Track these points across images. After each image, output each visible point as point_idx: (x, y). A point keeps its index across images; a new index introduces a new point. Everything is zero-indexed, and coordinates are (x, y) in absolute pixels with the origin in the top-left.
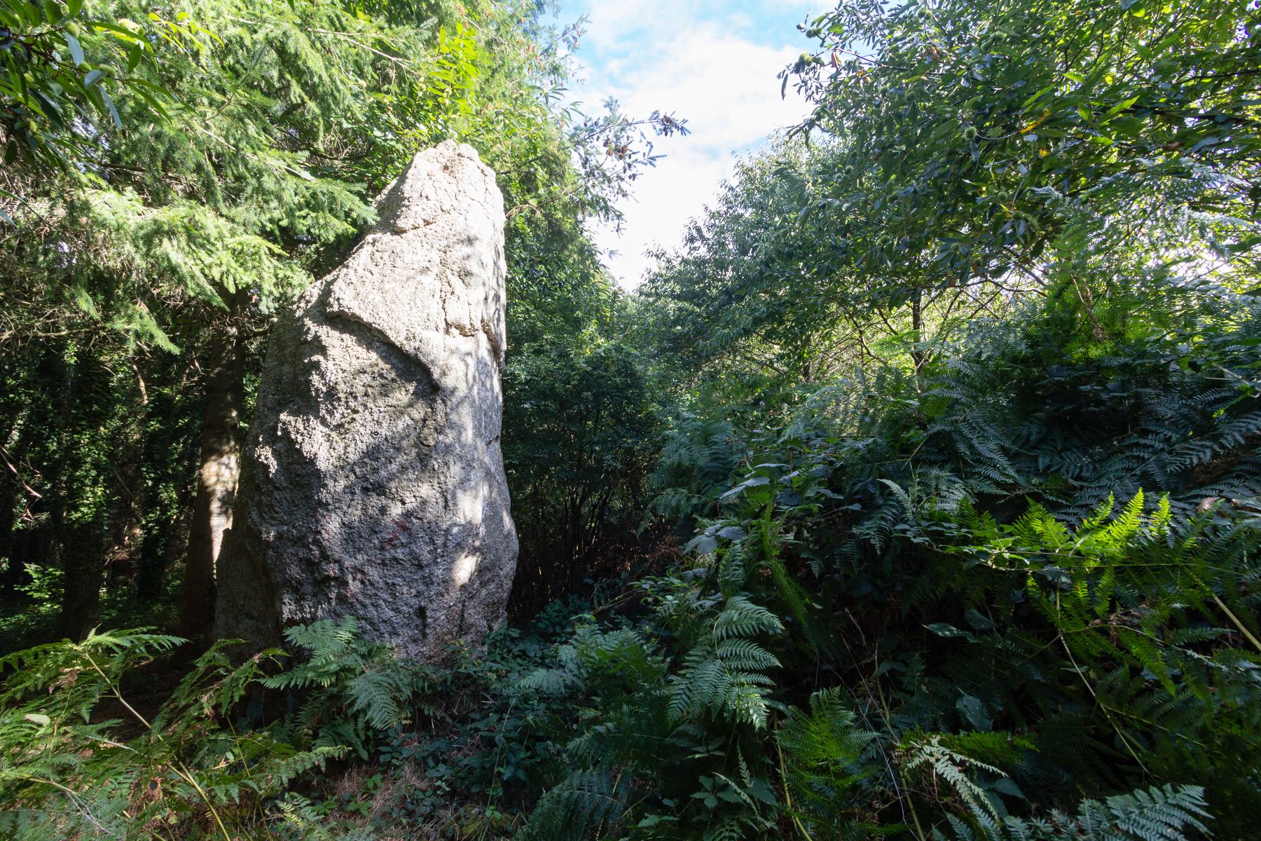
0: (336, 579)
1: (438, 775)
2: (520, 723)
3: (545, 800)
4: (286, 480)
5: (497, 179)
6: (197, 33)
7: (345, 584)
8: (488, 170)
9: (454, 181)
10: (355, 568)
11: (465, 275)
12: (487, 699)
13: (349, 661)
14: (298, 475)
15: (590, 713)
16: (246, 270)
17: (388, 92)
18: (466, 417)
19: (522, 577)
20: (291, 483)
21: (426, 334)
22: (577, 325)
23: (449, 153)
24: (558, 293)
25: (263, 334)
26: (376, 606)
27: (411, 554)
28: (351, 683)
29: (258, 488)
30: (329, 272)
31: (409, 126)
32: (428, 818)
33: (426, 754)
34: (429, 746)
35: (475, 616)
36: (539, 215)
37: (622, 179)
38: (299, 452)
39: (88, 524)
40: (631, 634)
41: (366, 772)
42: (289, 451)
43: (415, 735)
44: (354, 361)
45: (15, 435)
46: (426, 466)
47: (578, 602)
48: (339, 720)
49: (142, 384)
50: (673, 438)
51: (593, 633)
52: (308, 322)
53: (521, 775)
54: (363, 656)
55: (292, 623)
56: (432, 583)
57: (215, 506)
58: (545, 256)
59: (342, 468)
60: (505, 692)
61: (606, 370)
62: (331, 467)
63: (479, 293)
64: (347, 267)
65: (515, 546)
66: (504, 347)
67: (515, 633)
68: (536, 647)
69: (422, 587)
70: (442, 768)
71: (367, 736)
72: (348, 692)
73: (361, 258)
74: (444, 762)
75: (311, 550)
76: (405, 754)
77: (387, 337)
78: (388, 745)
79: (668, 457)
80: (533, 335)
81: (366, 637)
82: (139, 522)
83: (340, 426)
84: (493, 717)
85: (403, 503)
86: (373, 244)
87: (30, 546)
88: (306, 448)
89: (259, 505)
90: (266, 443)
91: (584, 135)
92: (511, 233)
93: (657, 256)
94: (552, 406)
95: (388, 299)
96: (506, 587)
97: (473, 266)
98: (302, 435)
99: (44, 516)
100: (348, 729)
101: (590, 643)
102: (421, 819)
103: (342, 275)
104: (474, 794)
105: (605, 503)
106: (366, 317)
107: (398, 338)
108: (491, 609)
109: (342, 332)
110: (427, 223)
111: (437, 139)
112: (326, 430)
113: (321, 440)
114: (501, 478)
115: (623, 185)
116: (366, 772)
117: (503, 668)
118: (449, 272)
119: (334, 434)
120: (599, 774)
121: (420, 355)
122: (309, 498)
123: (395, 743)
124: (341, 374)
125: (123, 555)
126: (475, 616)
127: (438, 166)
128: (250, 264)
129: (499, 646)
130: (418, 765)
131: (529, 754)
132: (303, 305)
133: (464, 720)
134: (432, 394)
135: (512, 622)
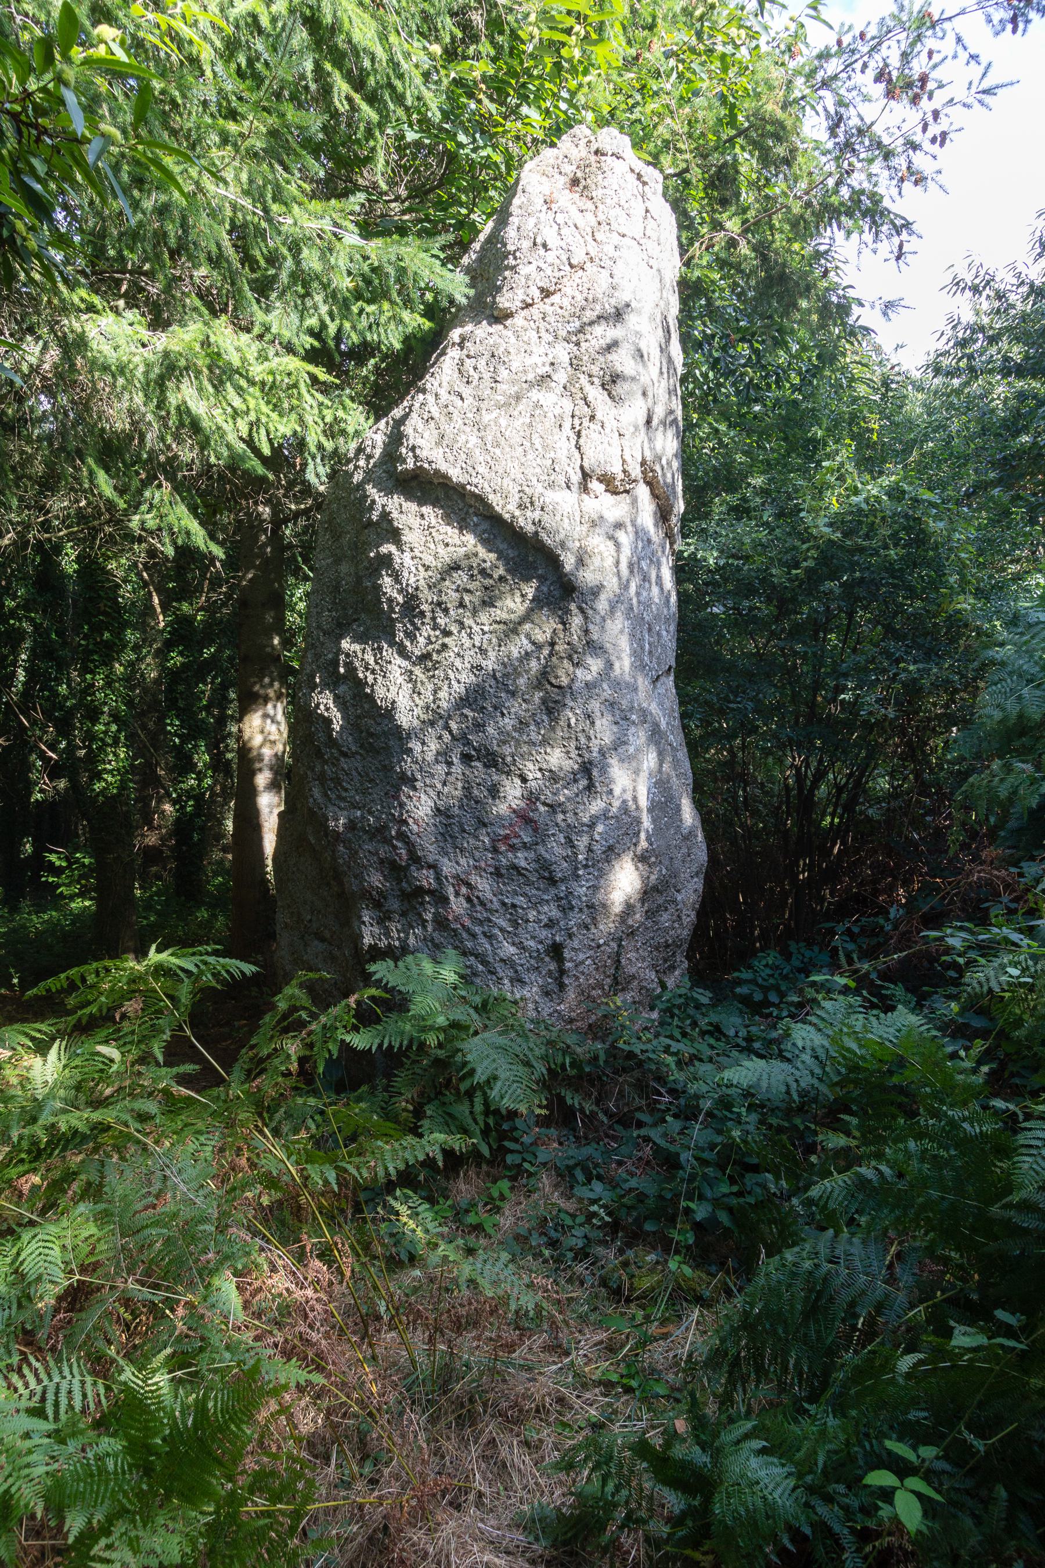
0: (431, 892)
1: (592, 1196)
2: (719, 1139)
3: (769, 1269)
4: (355, 741)
5: (666, 188)
6: (195, 23)
7: (445, 900)
8: (652, 174)
9: (589, 205)
10: (457, 877)
11: (611, 381)
12: (661, 1095)
13: (460, 1014)
14: (372, 735)
15: (836, 1141)
16: (281, 415)
17: (477, 56)
18: (617, 634)
19: (711, 905)
20: (362, 746)
21: (551, 497)
22: (812, 450)
23: (579, 153)
24: (774, 394)
25: (306, 512)
26: (490, 937)
27: (537, 861)
28: (465, 1046)
29: (319, 754)
30: (396, 403)
31: (513, 113)
32: (581, 1255)
33: (571, 1162)
34: (574, 1152)
35: (637, 963)
36: (744, 249)
37: (915, 147)
38: (371, 698)
39: (113, 796)
40: (913, 1019)
41: (488, 1174)
42: (358, 697)
43: (553, 1132)
44: (442, 551)
45: (21, 675)
46: (556, 720)
47: (808, 954)
48: (450, 1097)
49: (156, 600)
50: (1003, 664)
51: (850, 1010)
52: (371, 490)
53: (724, 1217)
54: (476, 1008)
55: (376, 954)
56: (572, 908)
57: (262, 779)
58: (755, 321)
59: (432, 723)
60: (693, 1088)
61: (867, 537)
62: (416, 722)
63: (635, 411)
64: (424, 391)
65: (701, 855)
66: (680, 507)
67: (704, 997)
68: (737, 1020)
69: (555, 913)
70: (598, 1187)
71: (487, 1124)
72: (458, 1058)
73: (445, 373)
74: (599, 1178)
75: (395, 847)
76: (542, 1158)
77: (489, 506)
78: (516, 1140)
79: (992, 705)
80: (728, 479)
81: (478, 981)
82: (169, 795)
83: (426, 657)
84: (673, 1124)
85: (524, 780)
86: (461, 345)
87: (52, 824)
88: (380, 692)
89: (322, 778)
90: (325, 685)
91: (833, 66)
92: (690, 290)
93: (976, 290)
94: (764, 609)
95: (489, 439)
96: (686, 920)
97: (623, 361)
98: (373, 672)
99: (62, 784)
100: (462, 1109)
101: (836, 1027)
102: (570, 1255)
103: (417, 405)
104: (648, 1234)
105: (858, 784)
106: (456, 474)
107: (506, 507)
108: (664, 954)
109: (421, 504)
110: (546, 293)
111: (556, 131)
112: (405, 663)
113: (400, 680)
114: (676, 738)
115: (920, 160)
116: (488, 1174)
117: (684, 1048)
118: (584, 380)
119: (417, 671)
120: (864, 1242)
121: (543, 536)
122: (388, 769)
123: (526, 1139)
124: (423, 573)
125: (152, 839)
126: (637, 963)
127: (562, 181)
128: (286, 405)
129: (675, 1013)
130: (559, 1175)
131: (735, 1189)
132: (362, 463)
133: (626, 1120)
134: (563, 598)
135: (698, 976)
